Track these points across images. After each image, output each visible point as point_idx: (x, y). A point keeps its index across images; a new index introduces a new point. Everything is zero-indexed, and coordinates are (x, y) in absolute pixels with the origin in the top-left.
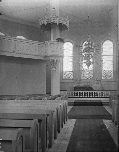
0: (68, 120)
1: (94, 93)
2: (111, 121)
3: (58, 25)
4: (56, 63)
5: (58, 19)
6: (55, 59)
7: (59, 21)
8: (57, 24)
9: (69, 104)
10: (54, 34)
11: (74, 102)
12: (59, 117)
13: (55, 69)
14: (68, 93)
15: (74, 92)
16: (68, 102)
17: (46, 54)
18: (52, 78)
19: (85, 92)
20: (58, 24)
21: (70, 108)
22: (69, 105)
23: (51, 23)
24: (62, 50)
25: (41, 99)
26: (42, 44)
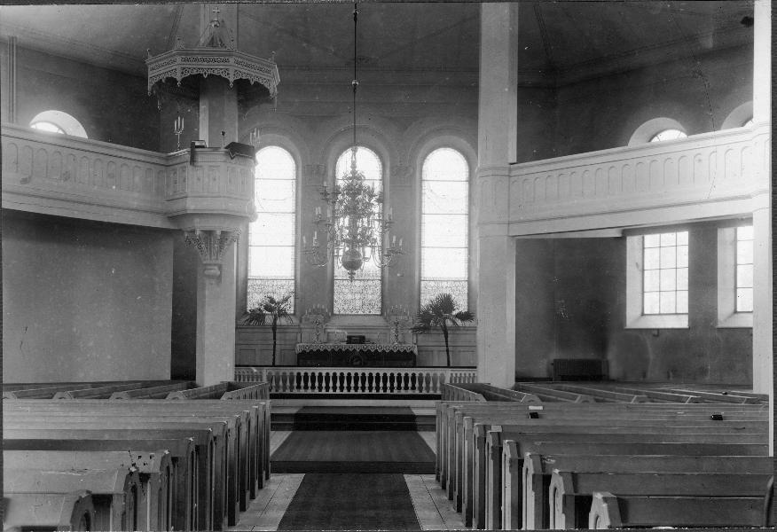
0: (271, 478)
1: (392, 375)
2: (433, 477)
3: (231, 84)
4: (221, 248)
5: (232, 60)
6: (217, 226)
7: (239, 68)
8: (227, 81)
9: (278, 422)
11: (296, 416)
12: (253, 445)
15: (296, 371)
16: (273, 407)
17: (176, 207)
18: (203, 307)
19: (346, 371)
20: (231, 80)
21: (277, 440)
22: (276, 427)
24: (245, 188)
26: (163, 162)
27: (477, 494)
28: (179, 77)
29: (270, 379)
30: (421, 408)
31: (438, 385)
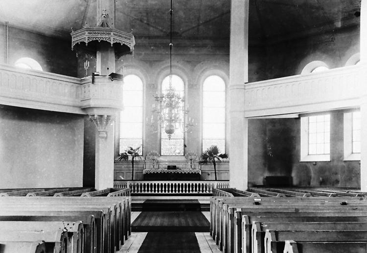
2: (209, 234)
4: (107, 124)
5: (112, 33)
7: (116, 37)
9: (135, 207)
10: (100, 64)
13: (105, 135)
14: (131, 184)
17: (85, 104)
20: (112, 43)
21: (134, 216)
22: (134, 210)
23: (122, 44)
25: (80, 195)
27: (230, 245)
28: (87, 42)
29: (131, 187)
30: (202, 200)
31: (211, 189)
